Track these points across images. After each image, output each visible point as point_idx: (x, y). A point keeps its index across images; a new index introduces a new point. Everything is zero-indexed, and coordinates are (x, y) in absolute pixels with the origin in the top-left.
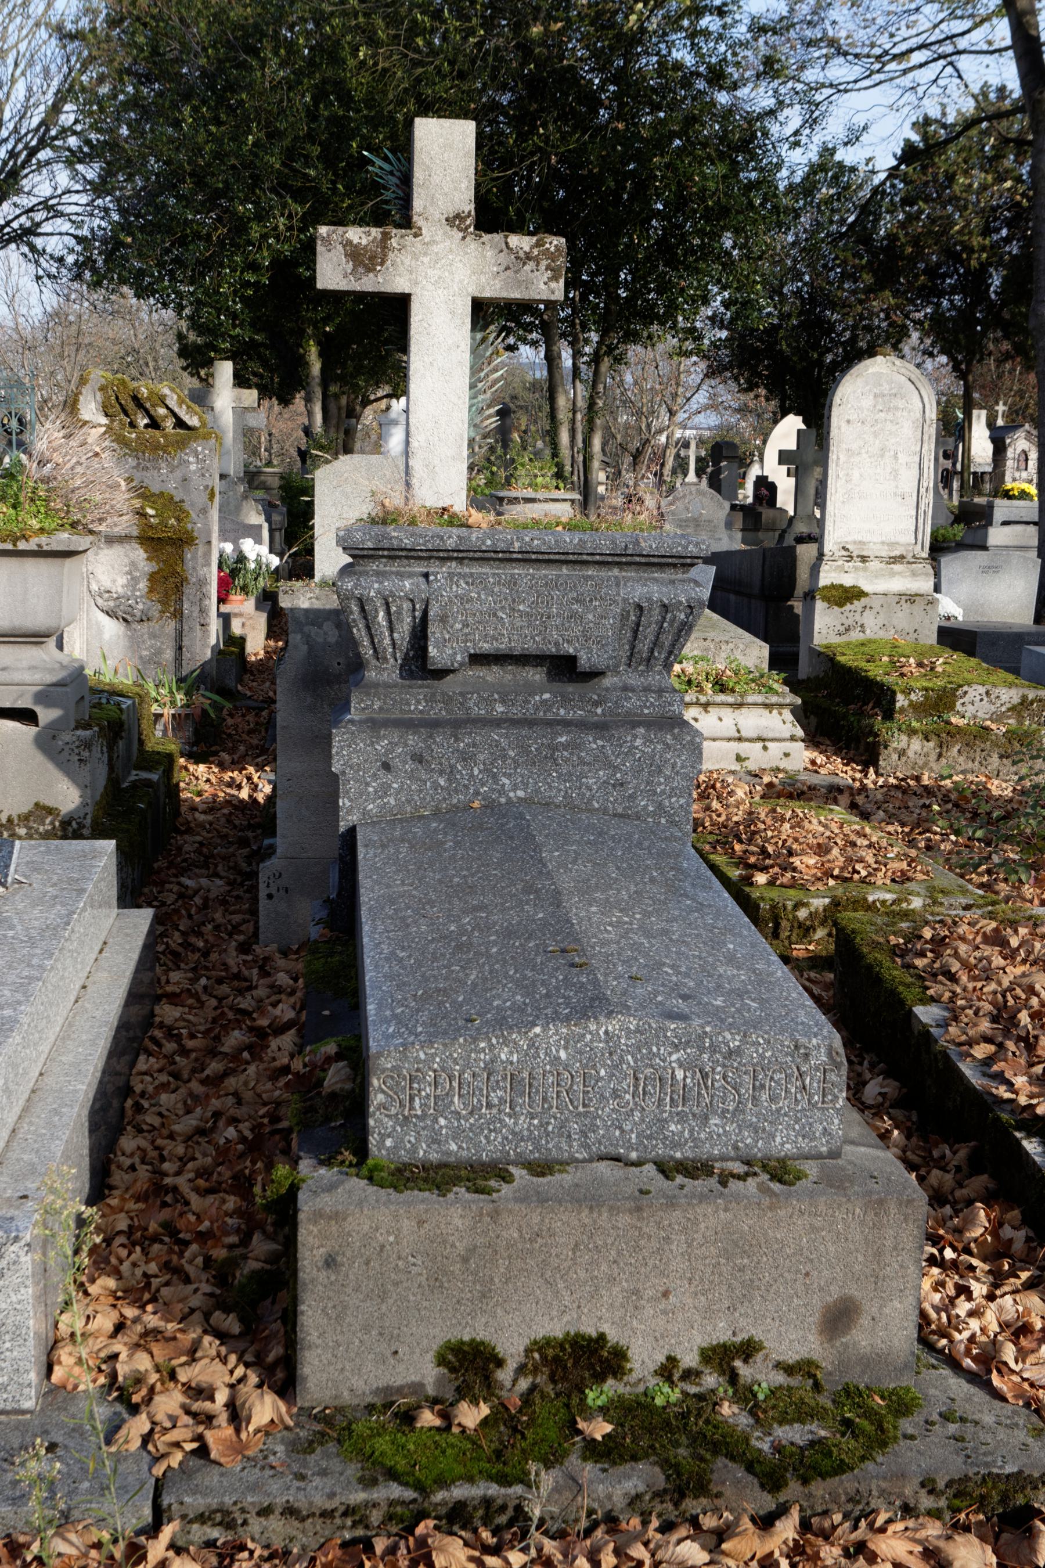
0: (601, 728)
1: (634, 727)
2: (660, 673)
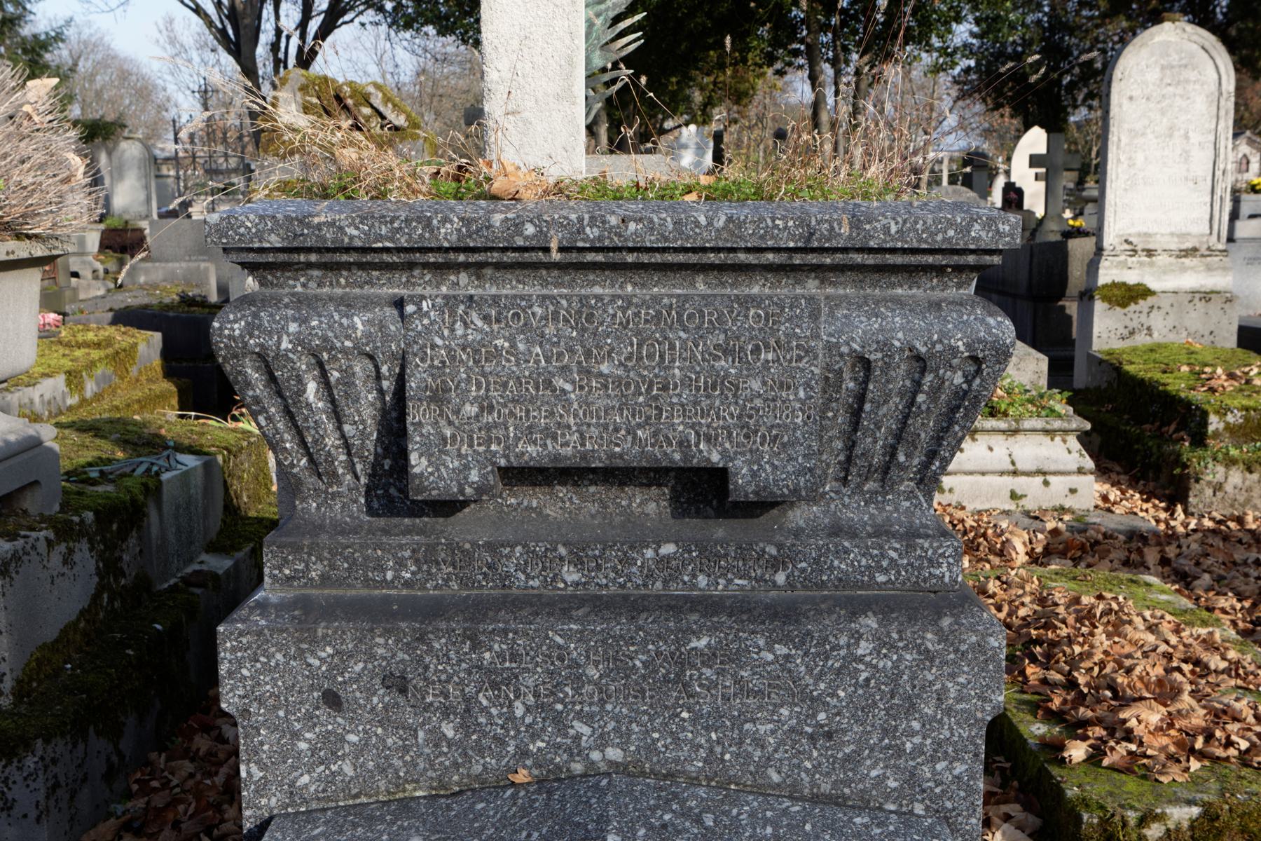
0: (783, 616)
1: (853, 616)
2: (910, 496)
